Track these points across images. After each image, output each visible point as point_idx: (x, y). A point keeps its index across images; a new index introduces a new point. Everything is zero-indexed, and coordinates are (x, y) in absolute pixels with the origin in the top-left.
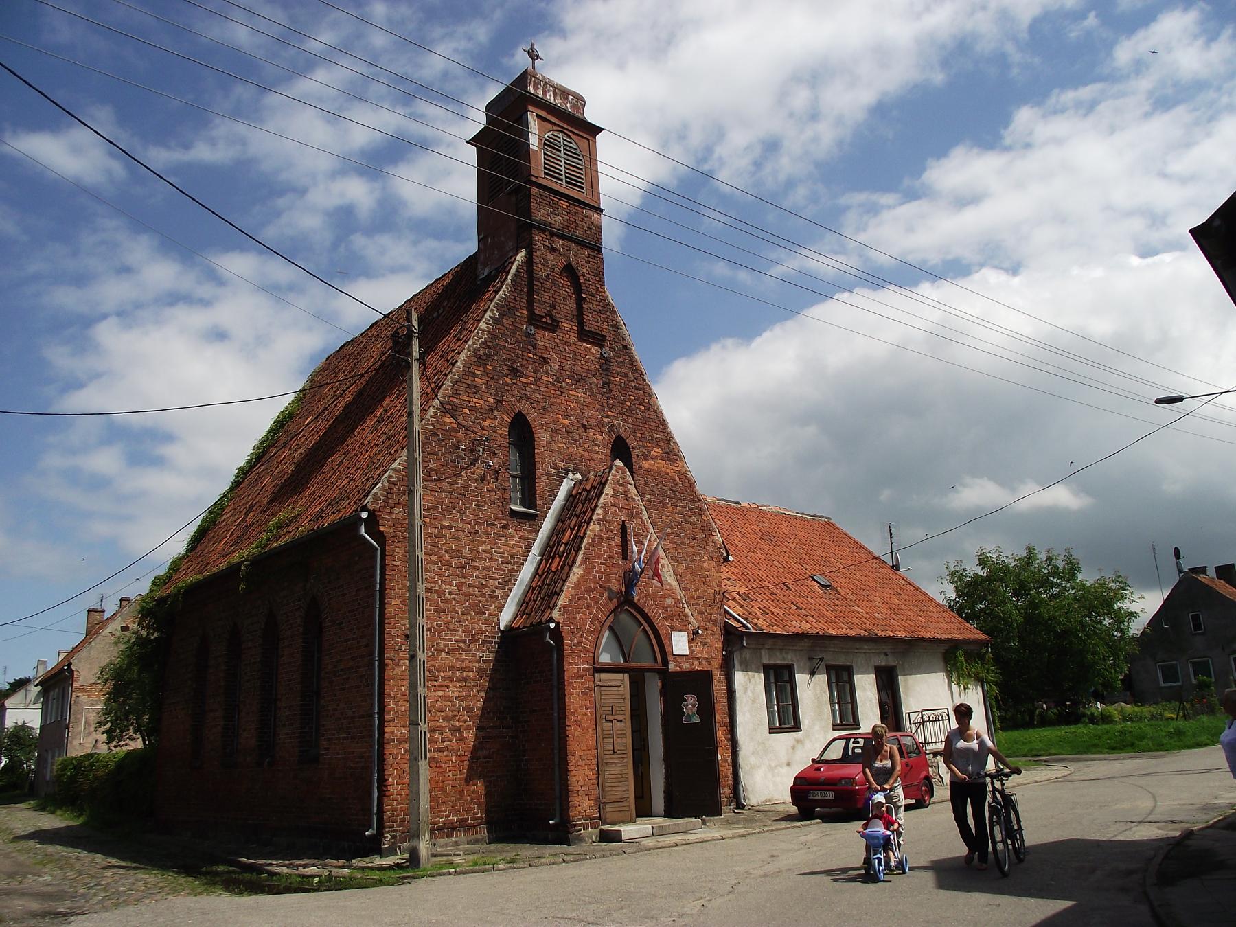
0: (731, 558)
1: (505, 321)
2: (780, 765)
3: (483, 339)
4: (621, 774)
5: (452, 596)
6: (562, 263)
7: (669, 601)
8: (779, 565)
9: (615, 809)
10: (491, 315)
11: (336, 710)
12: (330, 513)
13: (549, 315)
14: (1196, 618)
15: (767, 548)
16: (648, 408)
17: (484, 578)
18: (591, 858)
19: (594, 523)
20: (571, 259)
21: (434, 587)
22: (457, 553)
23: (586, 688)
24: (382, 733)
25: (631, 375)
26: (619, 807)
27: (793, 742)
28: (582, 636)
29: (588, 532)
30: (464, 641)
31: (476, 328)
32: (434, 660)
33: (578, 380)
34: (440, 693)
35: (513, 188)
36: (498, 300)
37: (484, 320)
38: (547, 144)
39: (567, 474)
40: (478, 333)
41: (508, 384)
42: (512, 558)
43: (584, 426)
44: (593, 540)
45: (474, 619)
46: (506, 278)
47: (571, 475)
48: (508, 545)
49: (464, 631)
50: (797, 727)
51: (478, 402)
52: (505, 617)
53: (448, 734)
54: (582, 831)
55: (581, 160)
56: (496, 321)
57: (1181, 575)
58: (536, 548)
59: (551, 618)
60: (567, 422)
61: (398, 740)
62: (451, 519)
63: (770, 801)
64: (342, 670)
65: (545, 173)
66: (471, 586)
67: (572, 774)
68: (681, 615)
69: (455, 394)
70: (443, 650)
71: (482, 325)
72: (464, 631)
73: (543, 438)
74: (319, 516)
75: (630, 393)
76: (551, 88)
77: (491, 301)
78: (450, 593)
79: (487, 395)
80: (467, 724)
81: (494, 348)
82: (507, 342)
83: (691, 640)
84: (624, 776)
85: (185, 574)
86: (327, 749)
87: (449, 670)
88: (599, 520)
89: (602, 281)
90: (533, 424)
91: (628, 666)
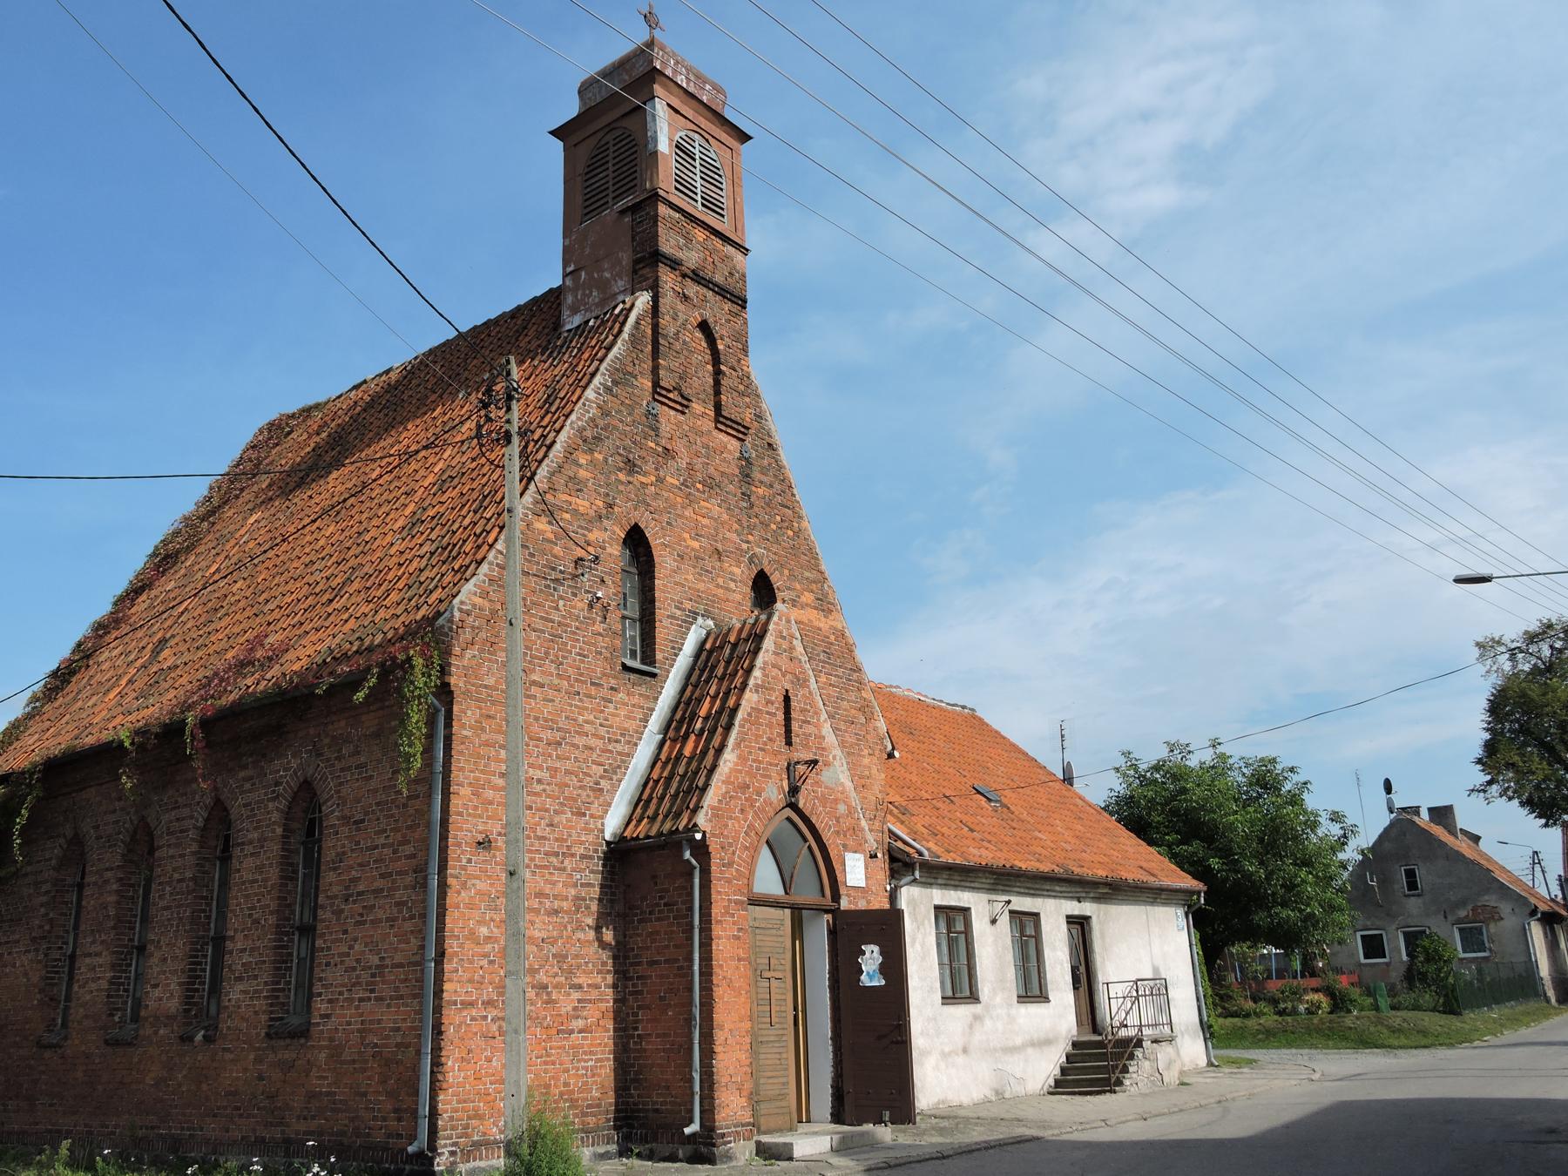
0: (897, 754)
1: (619, 391)
5: (542, 787)
6: (695, 318)
7: (842, 808)
8: (931, 770)
11: (348, 955)
13: (677, 389)
14: (1410, 874)
16: (797, 534)
17: (586, 761)
20: (708, 315)
22: (550, 724)
23: (740, 930)
24: (439, 992)
25: (777, 486)
28: (734, 853)
30: (556, 854)
33: (710, 485)
37: (592, 386)
40: (584, 405)
41: (622, 483)
42: (622, 735)
44: (749, 715)
45: (570, 821)
47: (700, 620)
48: (617, 715)
49: (557, 840)
50: (974, 998)
51: (582, 504)
52: (612, 822)
54: (732, 1144)
55: (720, 176)
56: (608, 390)
57: (1393, 816)
60: (696, 545)
61: (462, 1003)
62: (543, 673)
64: (359, 894)
65: (676, 188)
66: (568, 772)
67: (719, 1057)
68: (855, 829)
71: (590, 393)
72: (557, 840)
75: (776, 511)
78: (539, 781)
79: (594, 495)
80: (557, 979)
81: (605, 429)
82: (622, 421)
86: (328, 1016)
87: (535, 897)
89: (745, 351)
90: (652, 543)
91: (787, 899)
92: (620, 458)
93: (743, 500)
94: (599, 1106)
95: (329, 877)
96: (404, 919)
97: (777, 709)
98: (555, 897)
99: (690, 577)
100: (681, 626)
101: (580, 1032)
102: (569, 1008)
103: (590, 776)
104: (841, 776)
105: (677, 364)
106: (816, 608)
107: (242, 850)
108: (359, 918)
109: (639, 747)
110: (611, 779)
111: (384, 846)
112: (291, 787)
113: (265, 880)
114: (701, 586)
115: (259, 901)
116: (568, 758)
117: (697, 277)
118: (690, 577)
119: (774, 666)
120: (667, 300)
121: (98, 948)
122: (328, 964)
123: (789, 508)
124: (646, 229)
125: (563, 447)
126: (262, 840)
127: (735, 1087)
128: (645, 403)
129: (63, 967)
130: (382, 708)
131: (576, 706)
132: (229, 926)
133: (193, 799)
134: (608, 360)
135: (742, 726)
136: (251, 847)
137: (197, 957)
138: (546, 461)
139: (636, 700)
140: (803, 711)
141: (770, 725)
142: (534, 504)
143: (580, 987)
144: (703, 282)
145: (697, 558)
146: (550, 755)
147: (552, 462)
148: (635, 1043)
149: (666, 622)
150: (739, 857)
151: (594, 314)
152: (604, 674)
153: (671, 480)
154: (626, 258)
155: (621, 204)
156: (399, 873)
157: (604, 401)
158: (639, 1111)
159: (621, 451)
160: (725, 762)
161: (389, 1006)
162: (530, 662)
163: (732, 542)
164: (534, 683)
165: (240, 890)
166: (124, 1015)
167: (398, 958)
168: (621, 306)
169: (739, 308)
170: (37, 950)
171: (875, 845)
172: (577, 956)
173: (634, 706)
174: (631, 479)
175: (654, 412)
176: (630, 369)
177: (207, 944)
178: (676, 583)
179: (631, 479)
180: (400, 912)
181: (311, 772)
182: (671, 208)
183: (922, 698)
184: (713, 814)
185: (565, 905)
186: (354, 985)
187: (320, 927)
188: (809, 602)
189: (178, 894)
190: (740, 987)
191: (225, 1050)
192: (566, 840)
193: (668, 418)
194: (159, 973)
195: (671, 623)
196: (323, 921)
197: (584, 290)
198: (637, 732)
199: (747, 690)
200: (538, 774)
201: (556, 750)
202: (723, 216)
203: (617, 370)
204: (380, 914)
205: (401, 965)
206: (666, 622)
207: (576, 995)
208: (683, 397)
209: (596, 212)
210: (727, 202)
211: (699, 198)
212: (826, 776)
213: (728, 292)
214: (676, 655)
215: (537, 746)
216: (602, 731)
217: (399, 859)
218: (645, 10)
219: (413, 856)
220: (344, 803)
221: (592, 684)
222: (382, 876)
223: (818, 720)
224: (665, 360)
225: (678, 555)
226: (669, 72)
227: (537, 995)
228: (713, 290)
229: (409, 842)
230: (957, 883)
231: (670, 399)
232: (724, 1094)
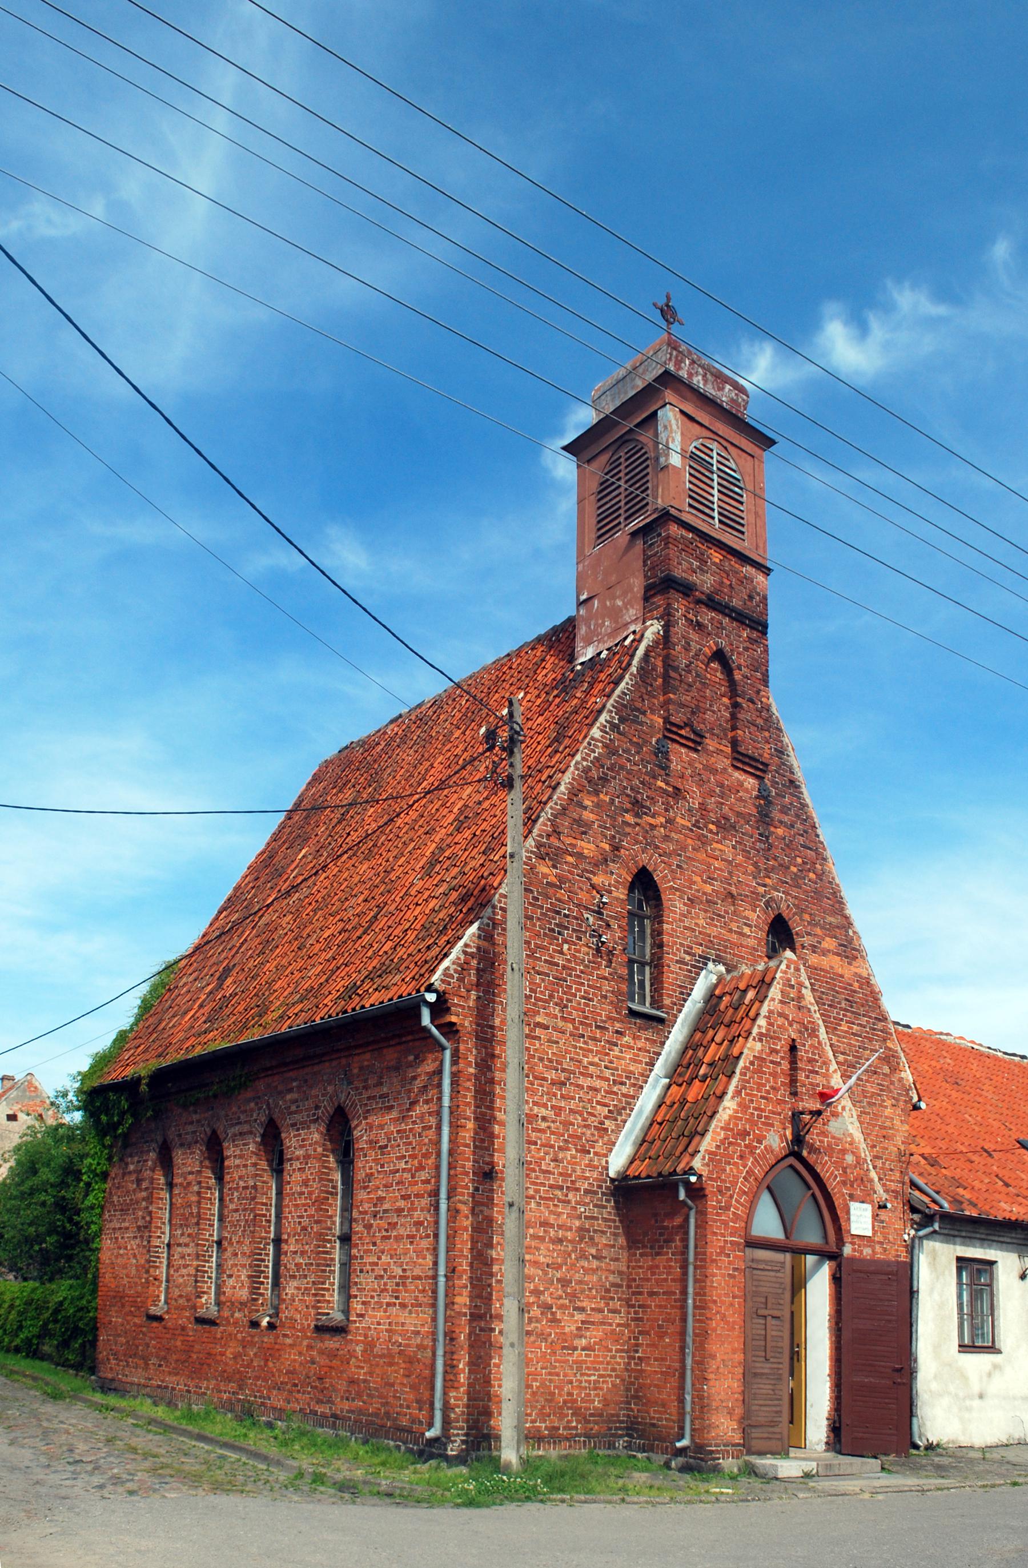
2: (971, 1397)
5: (546, 1124)
6: (710, 647)
10: (608, 718)
11: (377, 1264)
12: (371, 990)
15: (954, 1094)
16: (820, 876)
17: (590, 1101)
18: (753, 1500)
19: (754, 1039)
20: (723, 643)
22: (554, 1064)
23: (735, 1269)
27: (988, 1367)
28: (731, 1197)
29: (746, 1051)
30: (561, 1188)
31: (585, 737)
33: (725, 826)
35: (641, 525)
36: (619, 697)
37: (598, 724)
38: (697, 461)
39: (706, 964)
40: (589, 744)
41: (629, 825)
42: (627, 1077)
43: (731, 895)
44: (752, 1063)
45: (575, 1158)
46: (629, 665)
47: (710, 965)
49: (561, 1174)
51: (587, 847)
52: (617, 1161)
54: (721, 1461)
56: (614, 727)
58: (660, 1067)
59: (691, 1168)
60: (708, 888)
62: (547, 1015)
63: (953, 1442)
64: (385, 1211)
65: (690, 505)
68: (863, 1180)
69: (556, 832)
70: (533, 1197)
71: (596, 732)
72: (561, 1174)
73: (675, 905)
74: (352, 991)
76: (700, 370)
77: (609, 696)
78: (544, 1119)
80: (561, 1301)
82: (629, 760)
83: (875, 1217)
85: (132, 1055)
86: (362, 1316)
88: (761, 1034)
89: (765, 681)
90: (663, 886)
92: (627, 799)
93: (760, 841)
94: (601, 1415)
95: (361, 1195)
96: (421, 1238)
97: (782, 1058)
98: (560, 1227)
99: (701, 922)
100: (690, 971)
101: (583, 1349)
102: (573, 1328)
103: (595, 1116)
104: (850, 1127)
105: (689, 698)
106: (838, 955)
107: (291, 1165)
108: (384, 1234)
109: (645, 1090)
110: (616, 1120)
111: (404, 1170)
112: (327, 1111)
113: (310, 1193)
114: (714, 931)
115: (306, 1211)
116: (573, 1098)
117: (712, 603)
118: (701, 922)
119: (780, 1015)
120: (680, 627)
121: (186, 1240)
122: (361, 1271)
123: (811, 849)
124: (657, 552)
125: (567, 789)
126: (307, 1157)
127: (725, 1411)
128: (654, 740)
129: (162, 1253)
130: (399, 1044)
131: (581, 1048)
132: (283, 1231)
133: (252, 1116)
134: (615, 696)
135: (741, 1074)
136: (298, 1163)
137: (261, 1254)
138: (551, 804)
139: (640, 1044)
140: (810, 1061)
141: (774, 1075)
142: (537, 848)
143: (582, 1309)
144: (718, 607)
145: (708, 901)
146: (555, 1095)
147: (556, 804)
148: (636, 1364)
149: (675, 967)
151: (607, 646)
152: (609, 1018)
153: (683, 822)
154: (637, 584)
155: (635, 524)
156: (417, 1196)
157: (610, 740)
158: (638, 1423)
159: (629, 792)
160: (724, 1109)
161: (410, 1312)
162: (534, 1004)
163: (747, 885)
164: (538, 1025)
165: (290, 1200)
166: (210, 1298)
167: (417, 1272)
168: (631, 637)
169: (760, 635)
170: (142, 1237)
172: (580, 1282)
173: (639, 1049)
174: (639, 821)
175: (664, 750)
176: (639, 705)
177: (269, 1244)
178: (686, 928)
179: (639, 821)
180: (418, 1230)
181: (343, 1099)
182: (683, 527)
183: (976, 1047)
184: (710, 1159)
185: (569, 1235)
186: (382, 1291)
187: (354, 1238)
188: (831, 948)
189: (243, 1199)
190: (734, 1322)
191: (285, 1336)
192: (570, 1176)
193: (680, 757)
194: (232, 1266)
195: (680, 968)
196: (357, 1233)
197: (597, 620)
198: (642, 1075)
199: (751, 1039)
200: (543, 1112)
201: (561, 1090)
202: (743, 533)
203: (625, 706)
204: (402, 1231)
205: (419, 1278)
206: (675, 967)
207: (579, 1317)
208: (694, 732)
209: (607, 536)
210: (748, 518)
211: (716, 515)
212: (834, 1127)
213: (746, 618)
214: (685, 1000)
215: (542, 1086)
216: (607, 1073)
217: (416, 1183)
218: (662, 302)
219: (428, 1182)
220: (371, 1128)
221: (597, 1027)
222: (403, 1197)
223: (827, 1070)
224: (675, 694)
225: (689, 899)
226: (683, 374)
227: (542, 1314)
228: (730, 616)
229: (424, 1168)
230: (983, 1236)
231: (681, 736)
232: (714, 1417)
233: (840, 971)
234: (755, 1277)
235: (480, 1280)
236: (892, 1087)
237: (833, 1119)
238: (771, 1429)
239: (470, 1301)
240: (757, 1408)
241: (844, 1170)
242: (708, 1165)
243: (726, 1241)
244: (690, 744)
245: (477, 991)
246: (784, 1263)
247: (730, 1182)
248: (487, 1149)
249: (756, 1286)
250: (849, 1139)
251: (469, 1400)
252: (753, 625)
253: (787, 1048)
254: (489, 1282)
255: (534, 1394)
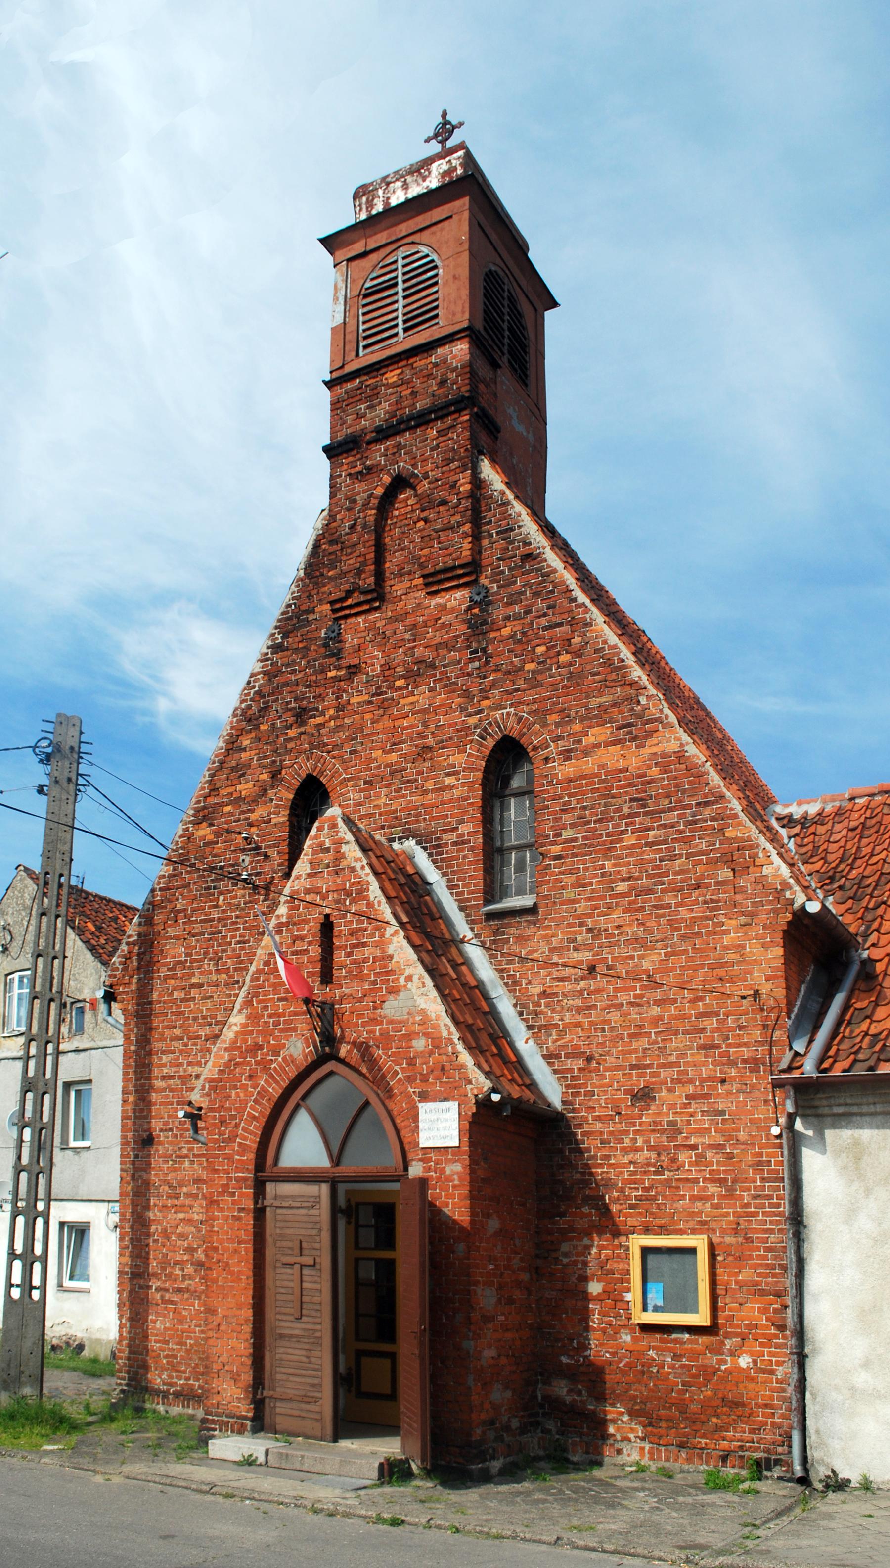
3: (257, 689)
4: (308, 1357)
9: (290, 1412)
21: (178, 1072)
23: (241, 1210)
26: (301, 1410)
28: (237, 1126)
32: (175, 1170)
34: (181, 1215)
53: (189, 1269)
60: (393, 757)
62: (201, 973)
70: (186, 1156)
84: (313, 1360)
87: (194, 1183)
150: (244, 1129)
164: (193, 986)
171: (487, 1085)
184: (211, 1088)
190: (239, 1271)
215: (195, 1044)
218: (453, 119)
227: (195, 1271)
231: (350, 607)
233: (621, 764)
234: (279, 1217)
235: (139, 1240)
236: (738, 897)
237: (391, 997)
238: (304, 1406)
239: (132, 1261)
240: (284, 1377)
241: (411, 1062)
242: (208, 1095)
243: (230, 1179)
244: (366, 607)
245: (138, 974)
246: (319, 1197)
247: (236, 1109)
248: (145, 1117)
249: (281, 1228)
250: (418, 1018)
251: (130, 1352)
252: (440, 413)
253: (317, 930)
254: (147, 1242)
255: (188, 1351)
